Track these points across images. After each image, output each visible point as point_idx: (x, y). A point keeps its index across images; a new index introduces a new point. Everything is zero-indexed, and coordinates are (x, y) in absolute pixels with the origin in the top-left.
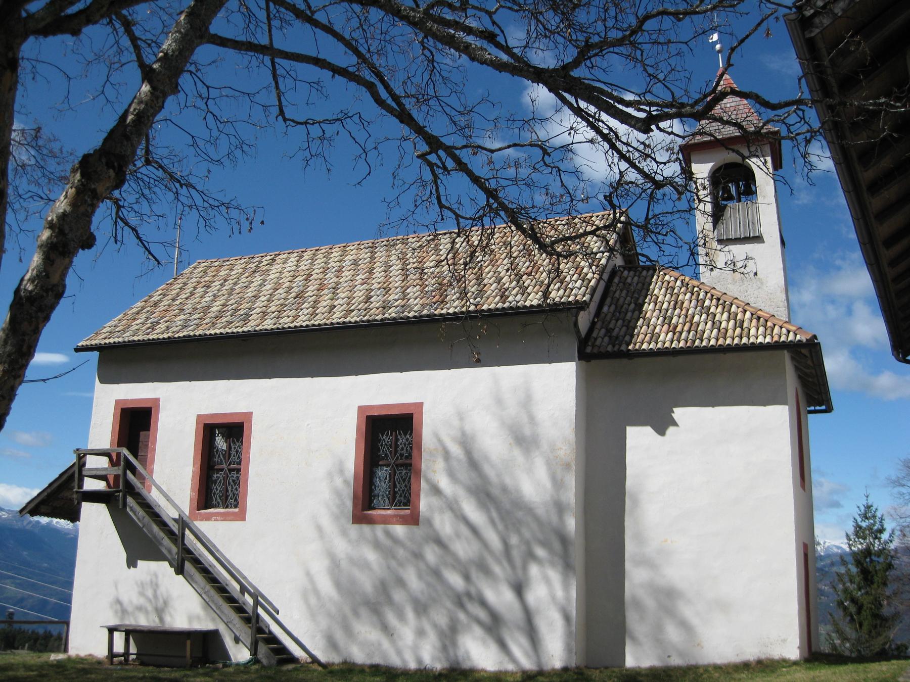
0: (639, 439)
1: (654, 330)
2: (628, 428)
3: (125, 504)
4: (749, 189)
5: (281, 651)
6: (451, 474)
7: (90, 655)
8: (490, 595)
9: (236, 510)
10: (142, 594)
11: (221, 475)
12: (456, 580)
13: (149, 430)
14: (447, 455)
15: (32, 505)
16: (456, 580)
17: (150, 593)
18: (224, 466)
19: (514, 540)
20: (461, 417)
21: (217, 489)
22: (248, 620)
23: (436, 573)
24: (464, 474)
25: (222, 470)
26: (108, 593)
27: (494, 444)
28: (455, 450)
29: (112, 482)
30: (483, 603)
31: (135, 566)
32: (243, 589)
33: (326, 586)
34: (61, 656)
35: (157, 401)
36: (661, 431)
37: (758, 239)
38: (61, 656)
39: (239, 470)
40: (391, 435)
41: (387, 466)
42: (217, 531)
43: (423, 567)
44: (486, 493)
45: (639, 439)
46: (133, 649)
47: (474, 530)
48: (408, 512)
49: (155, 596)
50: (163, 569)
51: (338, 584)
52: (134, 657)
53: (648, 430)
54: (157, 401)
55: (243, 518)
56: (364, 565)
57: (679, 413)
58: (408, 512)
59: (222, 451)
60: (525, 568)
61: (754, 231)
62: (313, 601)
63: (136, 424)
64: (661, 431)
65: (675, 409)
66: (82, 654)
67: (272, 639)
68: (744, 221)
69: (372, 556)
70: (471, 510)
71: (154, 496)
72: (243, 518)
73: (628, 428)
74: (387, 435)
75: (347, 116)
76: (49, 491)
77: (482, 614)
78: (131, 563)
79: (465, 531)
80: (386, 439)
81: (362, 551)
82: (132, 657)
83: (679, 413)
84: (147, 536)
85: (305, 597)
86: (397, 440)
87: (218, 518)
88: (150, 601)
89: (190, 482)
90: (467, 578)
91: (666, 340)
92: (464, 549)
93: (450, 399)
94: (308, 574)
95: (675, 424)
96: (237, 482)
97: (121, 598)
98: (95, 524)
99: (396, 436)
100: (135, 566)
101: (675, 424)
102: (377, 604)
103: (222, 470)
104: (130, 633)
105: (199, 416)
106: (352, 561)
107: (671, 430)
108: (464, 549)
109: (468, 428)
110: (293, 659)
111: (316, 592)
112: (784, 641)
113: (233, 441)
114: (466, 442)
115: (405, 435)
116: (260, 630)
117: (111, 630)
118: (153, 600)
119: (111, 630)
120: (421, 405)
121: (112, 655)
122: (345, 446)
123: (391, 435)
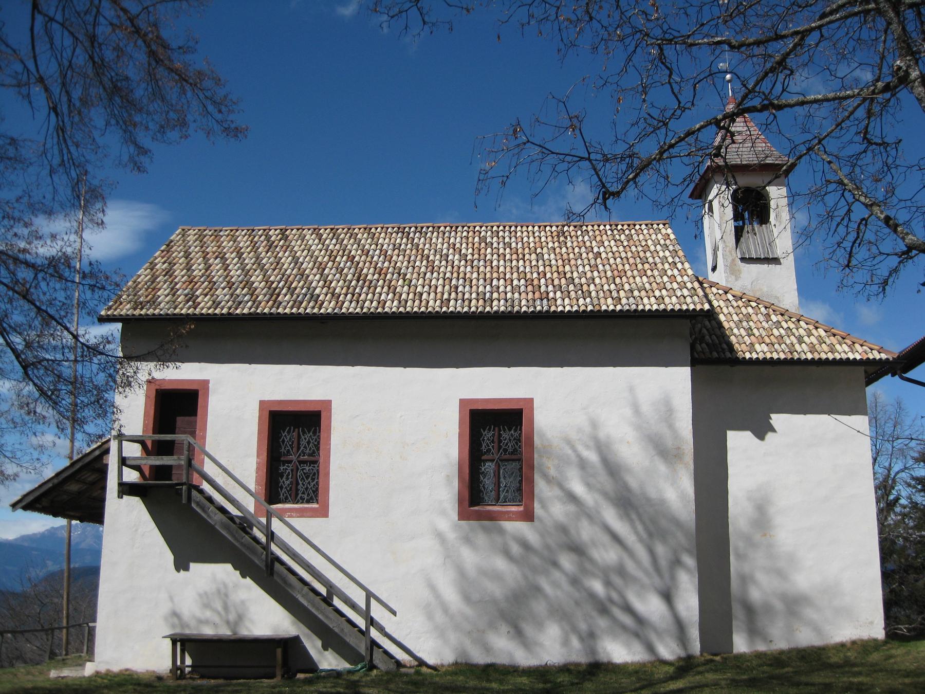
0: (738, 442)
2: (730, 434)
4: (762, 215)
7: (127, 670)
8: (639, 606)
9: (315, 506)
10: (207, 606)
11: (289, 468)
12: (598, 587)
13: (196, 415)
14: (583, 464)
15: (31, 498)
17: (219, 606)
18: (293, 457)
19: (660, 549)
20: (594, 425)
21: (285, 482)
24: (603, 478)
25: (290, 462)
26: (147, 597)
27: (632, 453)
28: (592, 456)
29: (147, 473)
30: (629, 609)
31: (187, 569)
33: (451, 595)
35: (205, 383)
36: (761, 436)
37: (776, 261)
39: (316, 462)
40: (494, 430)
41: (492, 461)
42: (296, 533)
44: (627, 501)
45: (738, 442)
46: (188, 661)
47: (616, 538)
48: (521, 508)
49: (226, 608)
50: (225, 572)
52: (190, 669)
53: (748, 434)
54: (205, 383)
55: (326, 515)
56: (496, 576)
58: (521, 508)
59: (294, 444)
60: (673, 578)
61: (772, 253)
62: (439, 617)
63: (177, 409)
64: (761, 436)
65: (772, 416)
68: (762, 243)
69: (500, 564)
70: (611, 516)
72: (326, 515)
73: (730, 434)
74: (489, 430)
75: (693, 104)
76: (56, 481)
78: (181, 565)
80: (487, 435)
81: (486, 558)
82: (188, 670)
86: (500, 435)
87: (294, 514)
88: (219, 613)
89: (254, 475)
90: (608, 583)
93: (565, 400)
94: (433, 588)
95: (773, 430)
96: (315, 475)
97: (178, 611)
98: (127, 524)
99: (500, 430)
100: (187, 569)
101: (773, 430)
102: (513, 612)
103: (290, 462)
105: (262, 403)
106: (483, 572)
107: (769, 435)
108: (608, 555)
109: (602, 435)
111: (445, 609)
112: (872, 623)
113: (303, 431)
114: (603, 448)
115: (510, 430)
118: (223, 613)
122: (446, 444)
123: (494, 430)
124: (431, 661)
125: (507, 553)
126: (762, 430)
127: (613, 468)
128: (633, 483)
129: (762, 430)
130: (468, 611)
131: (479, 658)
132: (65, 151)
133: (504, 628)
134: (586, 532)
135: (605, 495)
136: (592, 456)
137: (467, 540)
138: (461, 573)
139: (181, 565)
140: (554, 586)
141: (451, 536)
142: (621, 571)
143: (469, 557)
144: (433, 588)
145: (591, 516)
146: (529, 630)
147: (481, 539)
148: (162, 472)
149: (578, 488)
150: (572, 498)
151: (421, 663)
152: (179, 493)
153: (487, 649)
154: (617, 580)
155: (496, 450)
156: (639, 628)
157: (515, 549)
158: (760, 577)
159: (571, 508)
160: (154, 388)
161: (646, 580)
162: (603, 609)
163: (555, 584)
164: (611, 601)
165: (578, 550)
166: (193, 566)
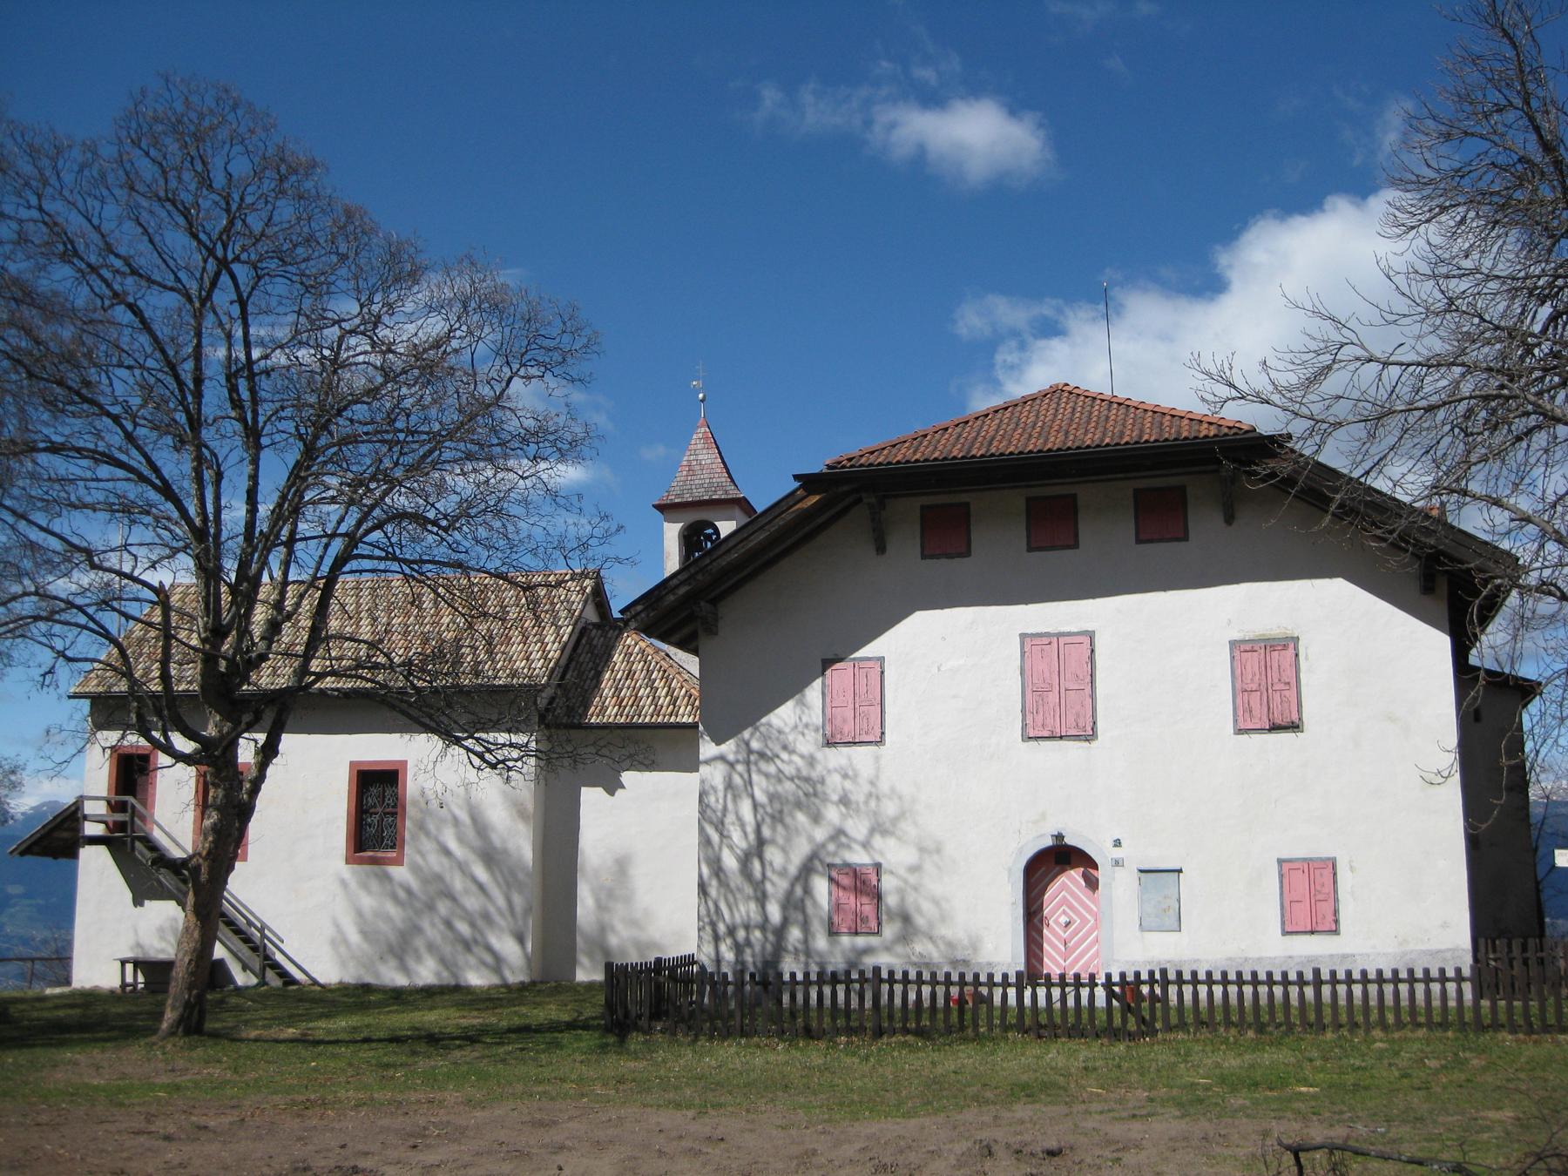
0: (591, 796)
1: (606, 708)
3: (133, 848)
5: (283, 974)
6: (461, 839)
8: (494, 941)
10: (162, 938)
12: (463, 928)
14: (456, 822)
16: (463, 928)
22: (255, 949)
23: (449, 924)
24: (471, 833)
28: (463, 816)
31: (142, 905)
32: (250, 923)
33: (354, 937)
34: (65, 990)
36: (611, 792)
38: (65, 990)
43: (437, 920)
44: (491, 856)
45: (591, 796)
46: (141, 979)
47: (481, 887)
51: (364, 933)
57: (627, 777)
62: (342, 949)
64: (611, 792)
66: (88, 985)
67: (276, 966)
69: (392, 909)
70: (481, 873)
71: (157, 834)
77: (489, 959)
78: (138, 901)
79: (474, 888)
83: (627, 777)
84: (147, 870)
85: (333, 943)
90: (473, 925)
91: (611, 714)
92: (472, 903)
94: (337, 925)
100: (142, 905)
101: (1059, 837)
102: (400, 948)
104: (137, 964)
107: (619, 792)
108: (472, 903)
110: (294, 981)
111: (345, 941)
116: (267, 957)
117: (123, 963)
119: (123, 963)
120: (404, 763)
121: (124, 985)
124: (322, 980)
125: (395, 898)
126: (612, 786)
127: (481, 827)
128: (497, 842)
129: (612, 786)
130: (365, 946)
131: (369, 979)
132: (210, 508)
133: (393, 963)
134: (458, 883)
135: (473, 849)
136: (463, 816)
137: (365, 886)
138: (359, 913)
139: (138, 901)
140: (432, 930)
141: (353, 885)
142: (486, 917)
143: (367, 902)
144: (337, 925)
145: (463, 868)
146: (411, 963)
147: (374, 885)
148: (121, 826)
149: (453, 845)
150: (447, 852)
151: (315, 982)
152: (125, 843)
153: (377, 974)
154: (480, 923)
155: (376, 807)
156: (498, 963)
157: (402, 894)
158: (619, 926)
159: (445, 861)
160: (120, 756)
161: (502, 923)
162: (467, 946)
163: (433, 925)
164: (476, 941)
165: (450, 896)
166: (147, 902)
